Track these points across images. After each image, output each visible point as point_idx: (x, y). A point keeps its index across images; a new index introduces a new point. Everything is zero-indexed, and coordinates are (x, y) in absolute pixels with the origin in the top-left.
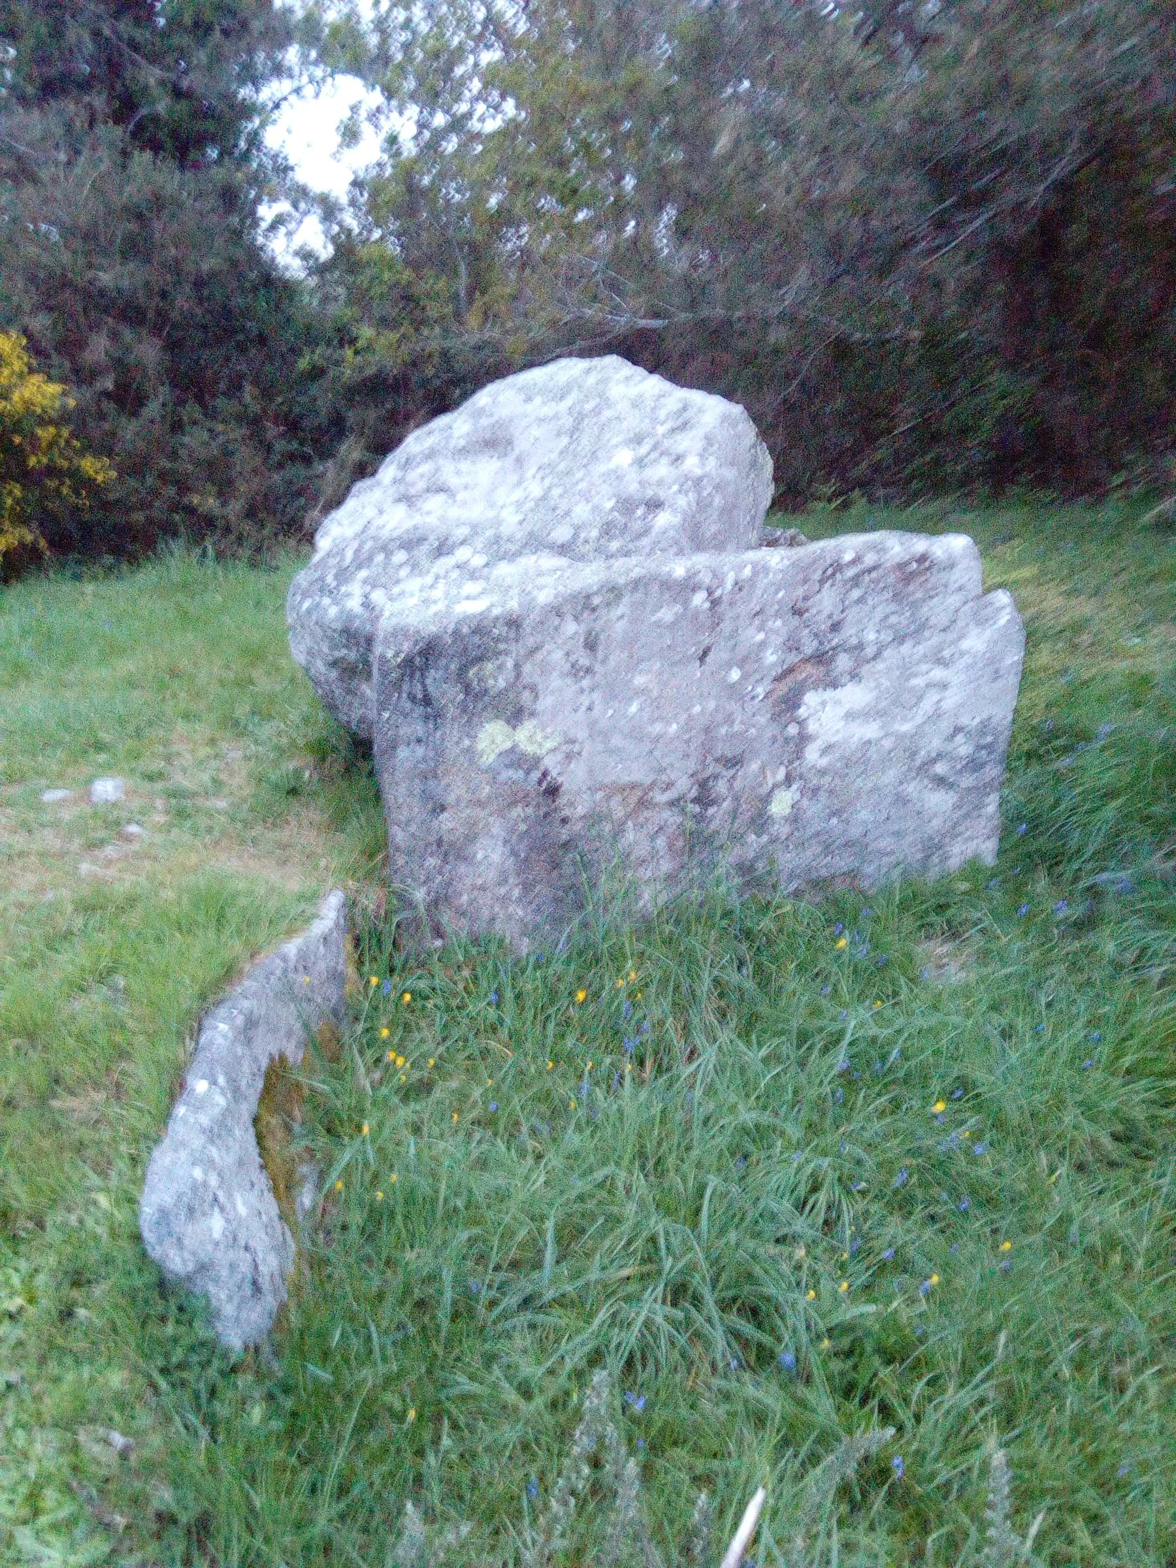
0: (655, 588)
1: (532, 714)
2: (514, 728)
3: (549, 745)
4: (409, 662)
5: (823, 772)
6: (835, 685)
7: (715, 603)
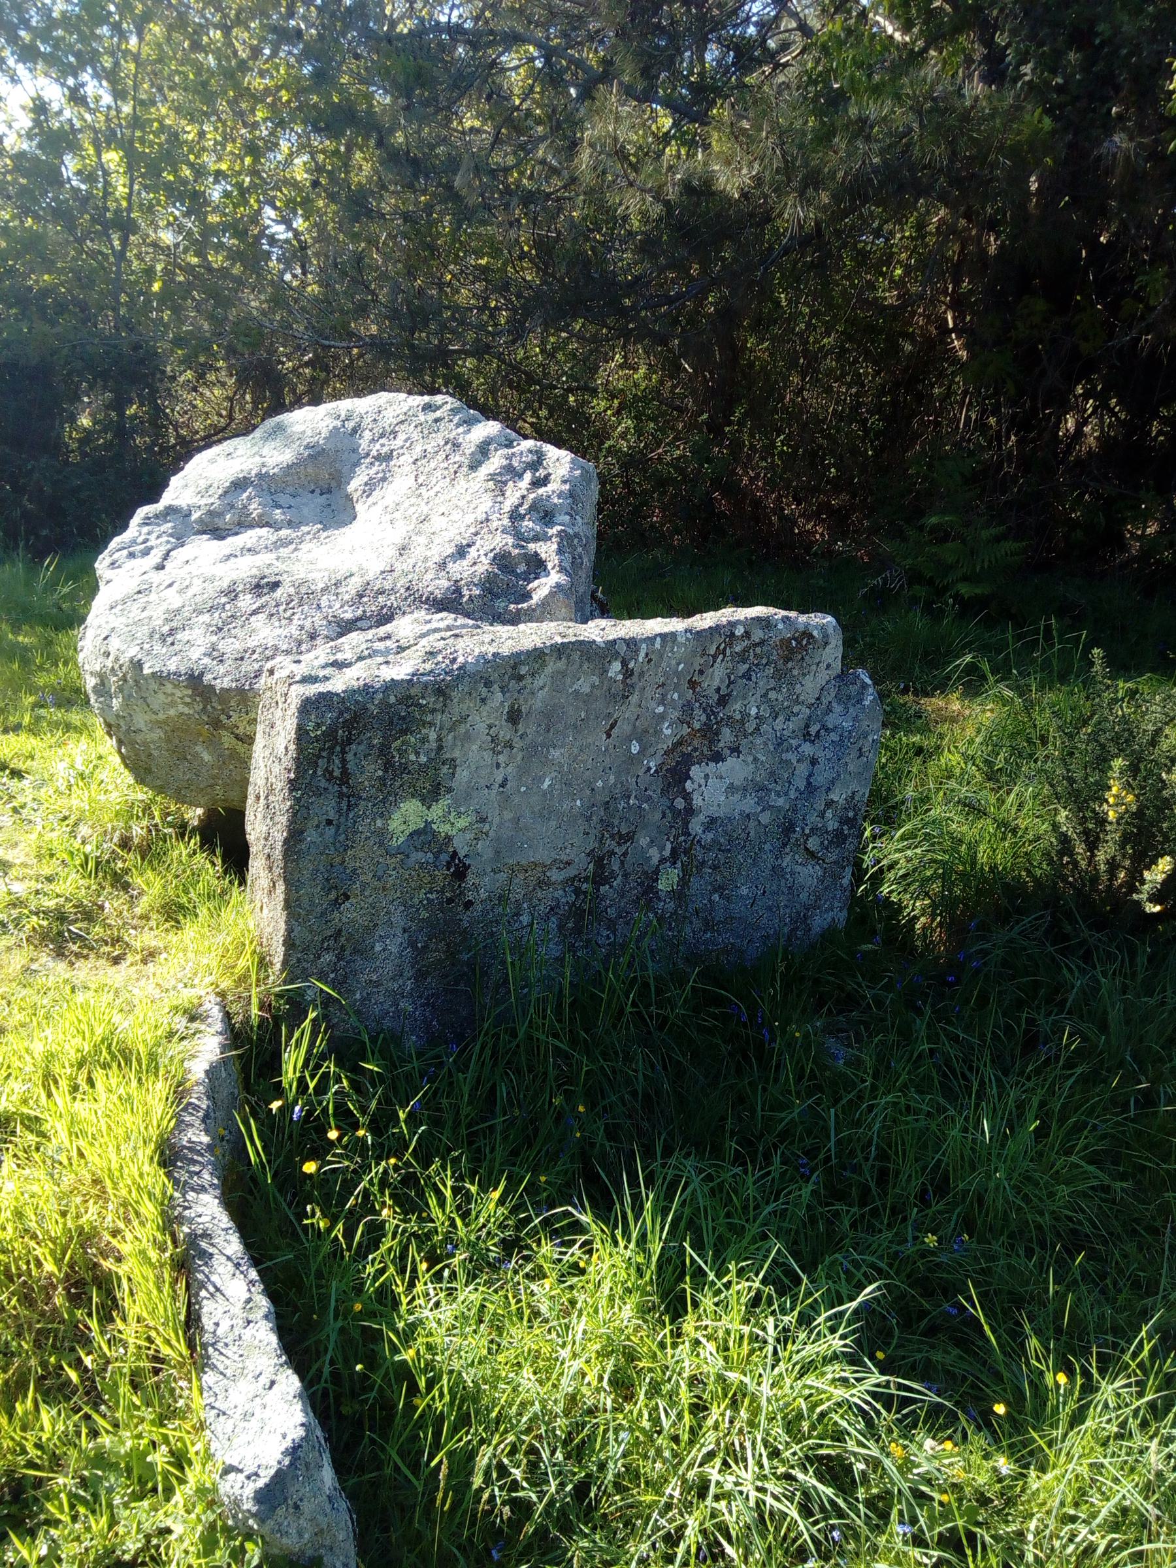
0: (576, 656)
1: (449, 790)
2: (429, 808)
3: (462, 823)
4: (331, 734)
5: (707, 849)
6: (718, 758)
7: (628, 673)
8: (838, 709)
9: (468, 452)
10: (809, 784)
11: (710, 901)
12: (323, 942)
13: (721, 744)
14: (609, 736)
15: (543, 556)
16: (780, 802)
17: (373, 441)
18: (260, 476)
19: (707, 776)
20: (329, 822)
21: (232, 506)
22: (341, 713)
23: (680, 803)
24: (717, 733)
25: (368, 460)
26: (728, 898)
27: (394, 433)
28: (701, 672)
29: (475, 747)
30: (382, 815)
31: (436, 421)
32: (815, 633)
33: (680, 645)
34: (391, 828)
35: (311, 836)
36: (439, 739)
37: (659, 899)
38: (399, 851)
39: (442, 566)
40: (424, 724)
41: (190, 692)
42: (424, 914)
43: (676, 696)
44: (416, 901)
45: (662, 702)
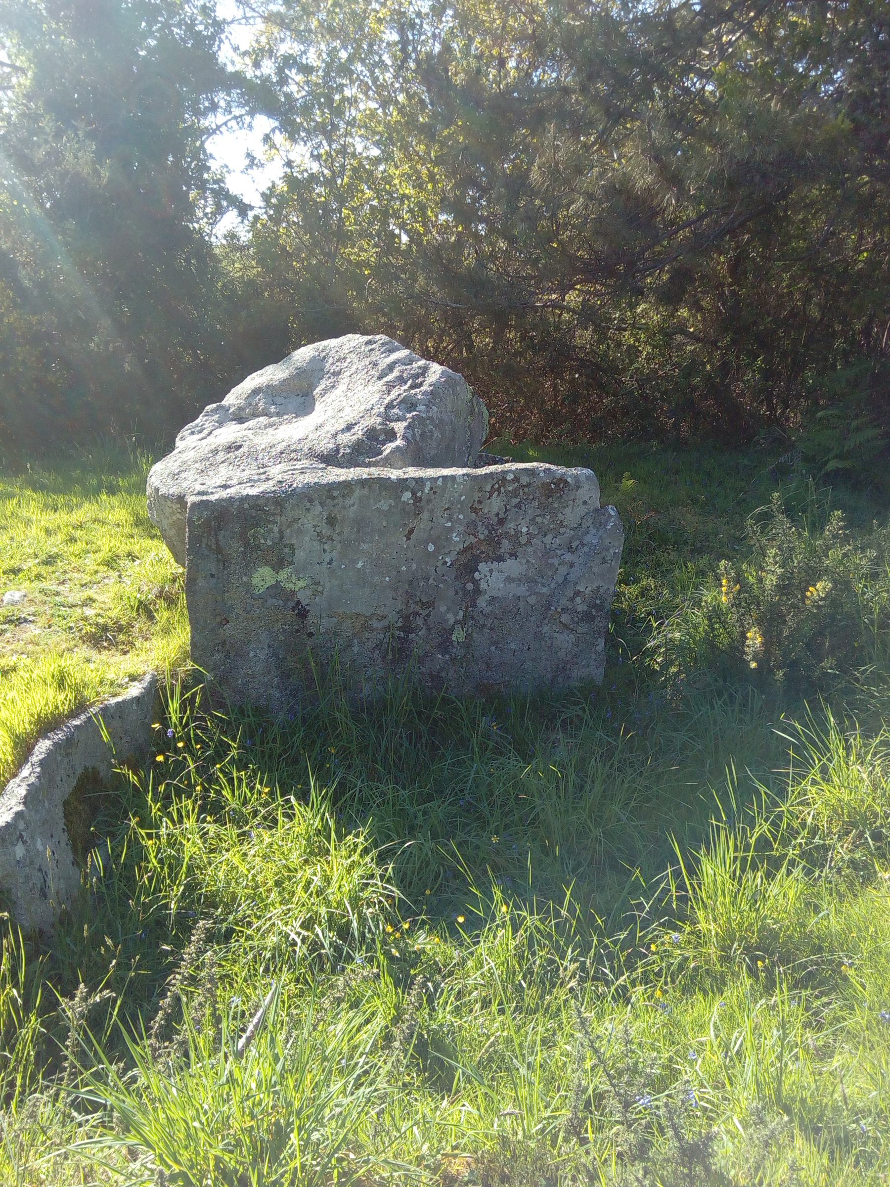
2: (277, 573)
3: (301, 583)
4: (207, 522)
5: (487, 616)
6: (500, 559)
7: (417, 500)
8: (593, 531)
9: (381, 368)
10: (566, 579)
11: (489, 650)
12: (214, 646)
13: (502, 550)
14: (408, 539)
15: (396, 430)
16: (544, 590)
17: (333, 364)
18: (268, 386)
19: (491, 571)
20: (212, 576)
21: (251, 405)
22: (213, 513)
23: (470, 586)
24: (499, 543)
25: (329, 375)
26: (502, 650)
27: (345, 358)
28: (480, 502)
29: (307, 539)
30: (246, 575)
31: (371, 350)
32: (569, 480)
33: (459, 484)
34: (254, 583)
35: (201, 583)
36: (281, 531)
37: (453, 646)
38: (260, 597)
39: (334, 436)
40: (269, 521)
41: (179, 506)
42: (282, 638)
43: (461, 516)
44: (276, 629)
45: (450, 519)
